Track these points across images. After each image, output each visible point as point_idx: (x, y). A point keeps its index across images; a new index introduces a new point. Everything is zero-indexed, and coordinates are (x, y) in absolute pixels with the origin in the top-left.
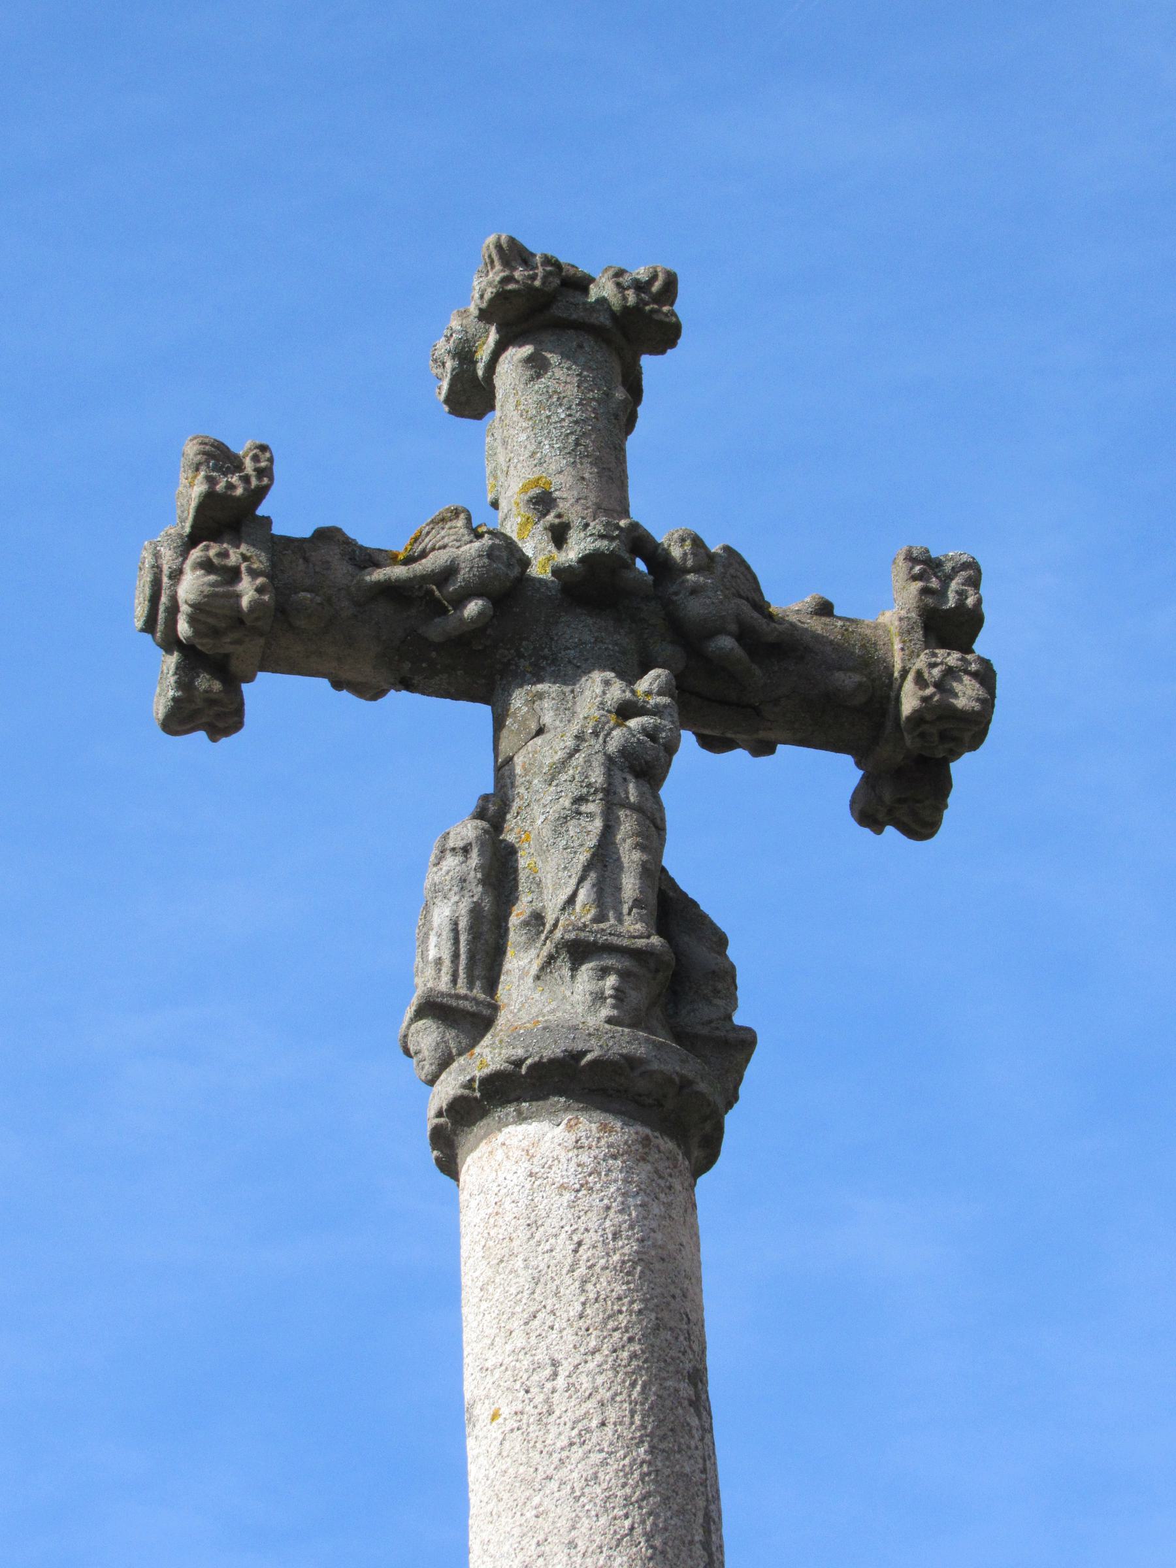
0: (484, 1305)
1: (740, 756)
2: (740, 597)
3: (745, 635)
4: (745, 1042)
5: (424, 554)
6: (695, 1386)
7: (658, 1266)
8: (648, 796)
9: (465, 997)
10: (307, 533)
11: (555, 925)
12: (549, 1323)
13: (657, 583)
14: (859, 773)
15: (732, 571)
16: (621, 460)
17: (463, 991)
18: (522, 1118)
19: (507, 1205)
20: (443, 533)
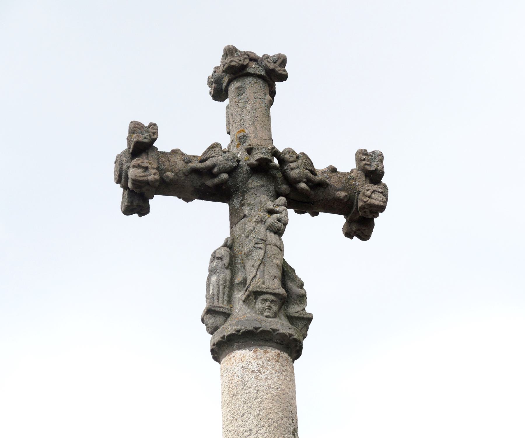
0: (228, 410)
1: (307, 215)
2: (307, 169)
3: (308, 181)
4: (309, 319)
5: (206, 159)
6: (294, 435)
7: (282, 396)
8: (279, 240)
9: (222, 307)
10: (169, 151)
11: (250, 285)
12: (249, 417)
13: (280, 166)
14: (345, 220)
15: (304, 161)
16: (268, 116)
17: (221, 305)
18: (239, 348)
19: (235, 377)
20: (213, 152)
